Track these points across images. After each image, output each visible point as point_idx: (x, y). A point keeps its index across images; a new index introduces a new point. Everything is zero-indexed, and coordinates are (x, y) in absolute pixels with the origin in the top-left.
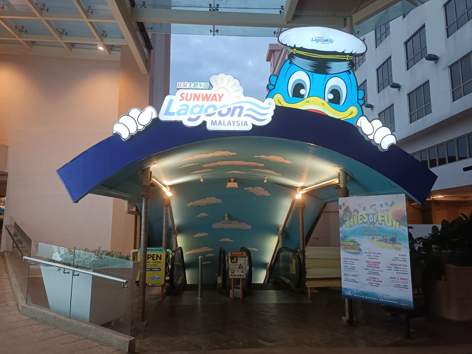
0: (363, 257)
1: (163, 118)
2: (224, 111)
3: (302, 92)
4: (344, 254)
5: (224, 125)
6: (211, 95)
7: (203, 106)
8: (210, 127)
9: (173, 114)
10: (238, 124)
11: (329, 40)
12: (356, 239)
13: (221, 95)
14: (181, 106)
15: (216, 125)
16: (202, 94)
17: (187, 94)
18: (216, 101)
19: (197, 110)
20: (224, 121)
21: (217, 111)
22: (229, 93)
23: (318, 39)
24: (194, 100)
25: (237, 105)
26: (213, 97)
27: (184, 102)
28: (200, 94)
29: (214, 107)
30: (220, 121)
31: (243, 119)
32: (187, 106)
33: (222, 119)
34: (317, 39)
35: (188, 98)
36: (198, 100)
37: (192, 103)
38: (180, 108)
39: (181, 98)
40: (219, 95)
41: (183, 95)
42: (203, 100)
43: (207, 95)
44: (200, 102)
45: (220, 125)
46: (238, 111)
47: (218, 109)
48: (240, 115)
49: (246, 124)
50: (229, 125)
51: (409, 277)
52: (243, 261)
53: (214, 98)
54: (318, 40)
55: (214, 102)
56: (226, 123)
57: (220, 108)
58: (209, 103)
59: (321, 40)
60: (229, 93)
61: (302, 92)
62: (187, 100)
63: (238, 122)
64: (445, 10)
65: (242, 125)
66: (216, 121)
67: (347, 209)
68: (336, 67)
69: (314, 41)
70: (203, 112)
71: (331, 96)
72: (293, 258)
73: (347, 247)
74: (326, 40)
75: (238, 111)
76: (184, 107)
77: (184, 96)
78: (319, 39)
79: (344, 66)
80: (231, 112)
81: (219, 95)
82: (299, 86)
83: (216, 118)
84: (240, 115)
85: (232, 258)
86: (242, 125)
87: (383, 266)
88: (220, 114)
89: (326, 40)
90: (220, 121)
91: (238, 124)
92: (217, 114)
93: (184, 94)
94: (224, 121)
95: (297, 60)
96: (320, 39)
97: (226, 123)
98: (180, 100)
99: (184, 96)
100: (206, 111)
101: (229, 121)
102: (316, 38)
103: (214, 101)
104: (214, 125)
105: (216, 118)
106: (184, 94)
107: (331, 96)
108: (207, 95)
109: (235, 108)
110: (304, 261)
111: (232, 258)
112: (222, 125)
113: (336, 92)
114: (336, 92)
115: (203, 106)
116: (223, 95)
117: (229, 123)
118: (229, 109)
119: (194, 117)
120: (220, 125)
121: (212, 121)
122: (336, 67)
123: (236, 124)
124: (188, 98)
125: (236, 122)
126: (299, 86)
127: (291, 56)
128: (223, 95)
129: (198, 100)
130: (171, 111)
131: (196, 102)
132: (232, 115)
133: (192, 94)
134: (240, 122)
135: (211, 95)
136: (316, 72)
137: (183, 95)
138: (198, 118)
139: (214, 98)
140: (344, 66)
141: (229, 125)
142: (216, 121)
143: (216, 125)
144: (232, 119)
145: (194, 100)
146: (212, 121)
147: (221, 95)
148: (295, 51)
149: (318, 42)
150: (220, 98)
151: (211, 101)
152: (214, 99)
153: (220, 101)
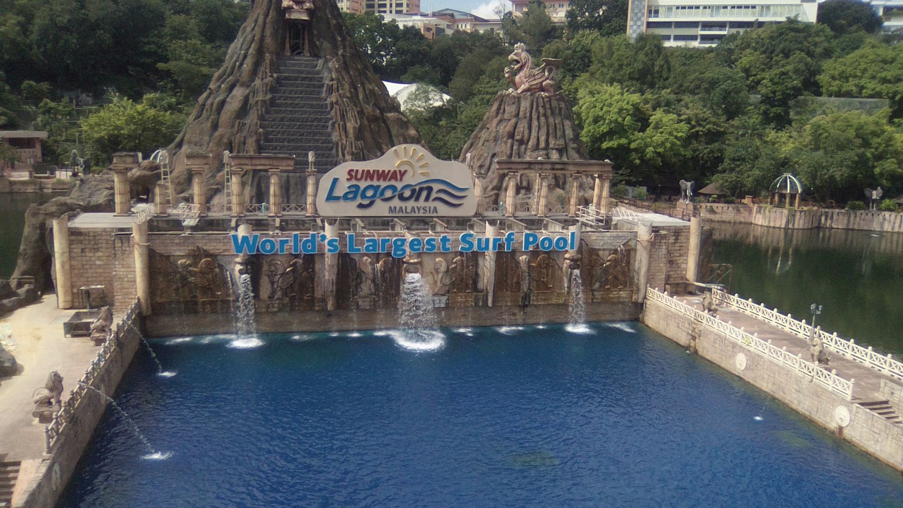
11: (436, 187)
14: (349, 187)
21: (397, 193)
23: (369, 183)
25: (425, 185)
27: (354, 182)
29: (394, 188)
30: (401, 208)
32: (357, 187)
34: (363, 184)
35: (359, 176)
36: (372, 179)
39: (349, 177)
42: (378, 179)
46: (424, 194)
48: (427, 199)
54: (370, 193)
55: (393, 183)
56: (409, 210)
58: (387, 183)
59: (388, 194)
64: (660, 27)
69: (345, 197)
70: (378, 195)
72: (610, 60)
74: (421, 190)
75: (424, 194)
76: (353, 189)
78: (375, 183)
84: (427, 199)
89: (421, 190)
90: (401, 208)
96: (383, 184)
97: (409, 210)
99: (353, 174)
100: (382, 194)
102: (354, 182)
115: (379, 186)
116: (405, 171)
117: (413, 209)
118: (413, 191)
121: (390, 207)
123: (422, 211)
128: (405, 171)
129: (372, 179)
131: (369, 183)
132: (417, 199)
134: (428, 209)
142: (395, 207)
146: (390, 207)
149: (366, 202)
151: (390, 180)
153: (401, 180)
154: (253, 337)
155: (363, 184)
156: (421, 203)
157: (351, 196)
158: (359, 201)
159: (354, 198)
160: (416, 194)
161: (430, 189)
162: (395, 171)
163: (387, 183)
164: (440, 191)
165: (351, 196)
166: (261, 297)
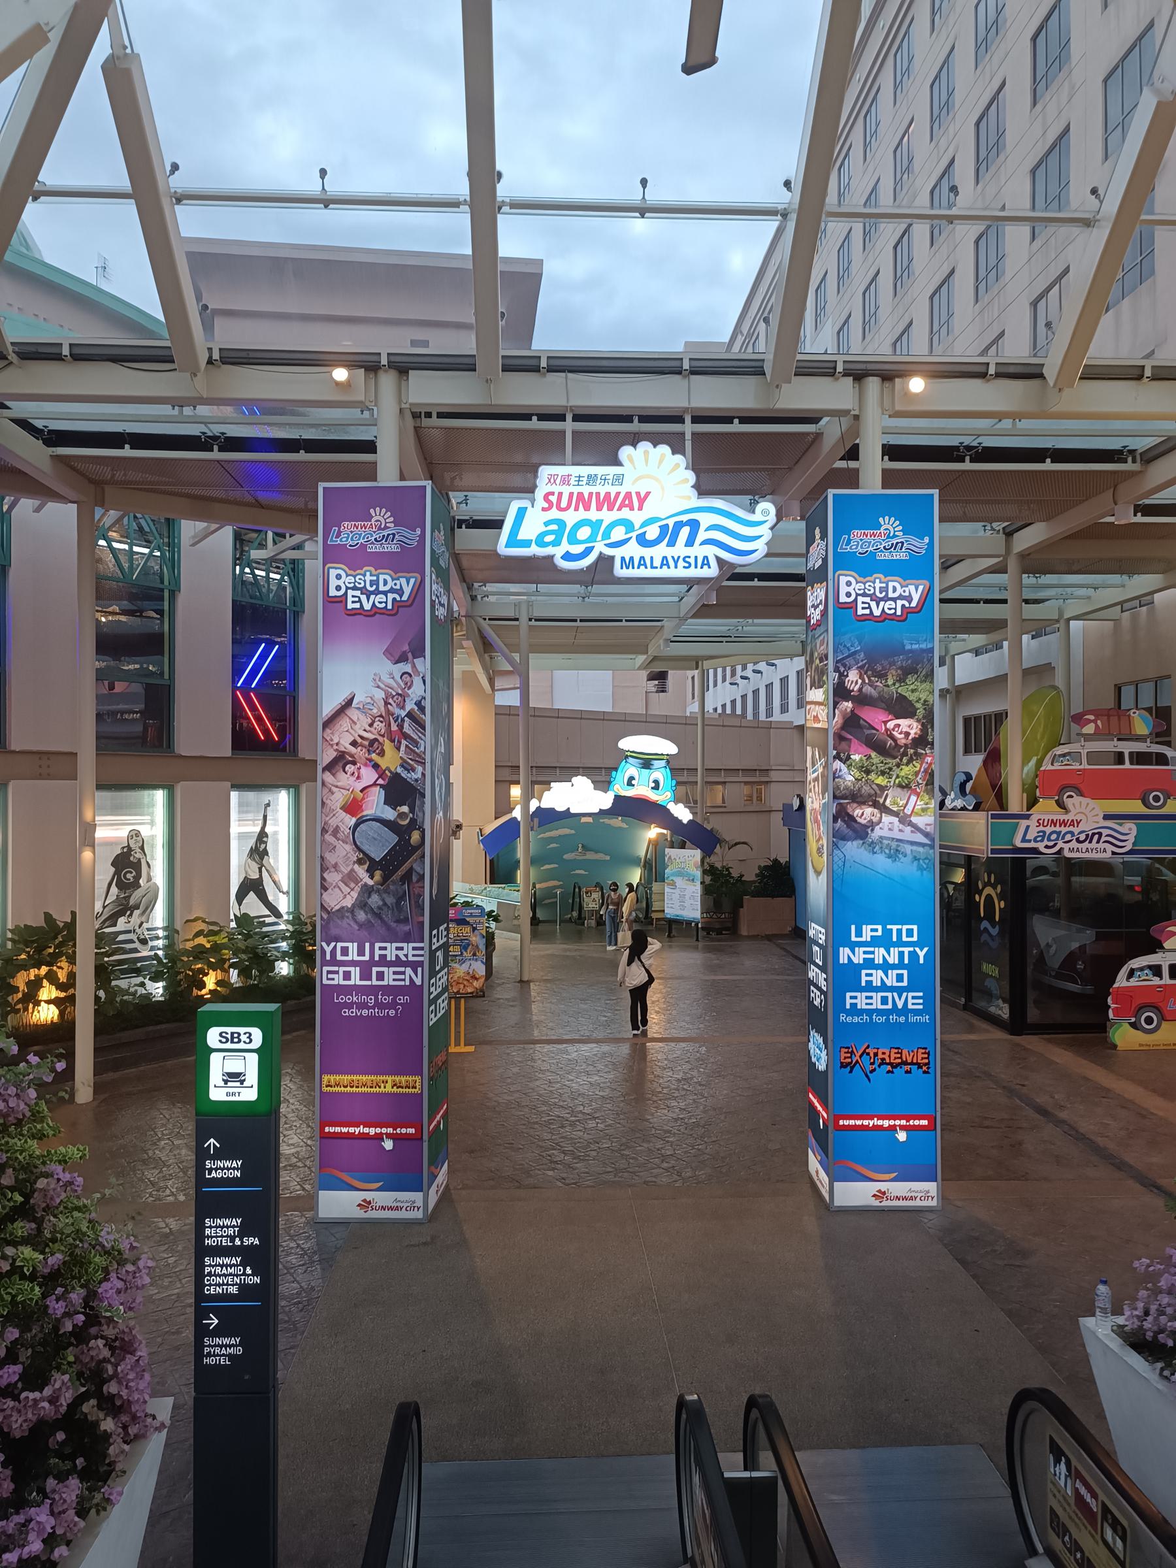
0: (677, 891)
1: (543, 806)
2: (652, 533)
3: (633, 782)
4: (667, 890)
5: (652, 567)
6: (618, 494)
7: (601, 521)
8: (572, 811)
9: (527, 543)
10: (687, 565)
11: (1105, 832)
12: (674, 878)
13: (642, 495)
14: (546, 524)
15: (633, 568)
16: (598, 494)
17: (560, 494)
18: (632, 509)
19: (584, 533)
20: (652, 558)
21: (634, 534)
22: (663, 489)
23: (1053, 828)
24: (576, 509)
25: (685, 518)
26: (624, 500)
27: (554, 514)
28: (591, 494)
30: (642, 558)
31: (699, 551)
32: (561, 523)
33: (647, 552)
34: (1048, 830)
35: (564, 504)
37: (571, 517)
38: (544, 529)
39: (546, 505)
40: (638, 494)
41: (551, 497)
43: (608, 494)
44: (593, 514)
45: (642, 567)
46: (685, 532)
47: (636, 528)
48: (690, 543)
49: (706, 562)
50: (665, 567)
51: (699, 903)
52: (596, 895)
53: (627, 502)
55: (626, 513)
56: (657, 563)
57: (642, 526)
58: (615, 515)
59: (1068, 837)
60: (663, 489)
61: (633, 782)
62: (559, 509)
63: (687, 559)
65: (696, 567)
66: (632, 558)
67: (670, 858)
68: (657, 764)
70: (599, 537)
71: (653, 785)
73: (669, 884)
75: (685, 532)
76: (554, 527)
77: (554, 499)
78: (1057, 829)
79: (663, 763)
80: (669, 534)
81: (638, 494)
82: (631, 778)
83: (633, 550)
84: (690, 543)
85: (587, 893)
86: (696, 567)
87: (687, 897)
88: (642, 541)
90: (642, 558)
91: (687, 565)
92: (634, 540)
93: (553, 494)
94: (652, 558)
95: (630, 760)
97: (657, 563)
98: (544, 509)
99: (554, 499)
100: (607, 535)
101: (665, 558)
102: (1041, 828)
103: (626, 510)
104: (628, 568)
105: (633, 550)
106: (553, 494)
107: (653, 785)
108: (608, 494)
109: (679, 526)
110: (651, 894)
111: (587, 893)
112: (646, 568)
113: (656, 782)
114: (656, 782)
115: (601, 521)
116: (648, 494)
117: (665, 562)
118: (664, 529)
119: (577, 549)
120: (642, 567)
121: (623, 559)
122: (657, 764)
123: (681, 563)
124: (564, 504)
125: (681, 559)
126: (631, 778)
127: (627, 757)
128: (648, 494)
130: (522, 536)
131: (582, 514)
132: (671, 543)
133: (571, 495)
134: (692, 560)
135: (618, 494)
136: (643, 768)
137: (551, 497)
138: (588, 551)
139: (627, 502)
140: (663, 763)
141: (665, 567)
142: (632, 558)
143: (633, 568)
144: (670, 552)
145: (576, 509)
146: (623, 559)
147: (642, 495)
148: (629, 754)
149: (1051, 844)
150: (642, 501)
151: (619, 509)
152: (626, 506)
153: (640, 508)
154: (696, 948)
155: (1048, 830)
156: (1094, 844)
157: (1039, 839)
158: (1046, 842)
159: (1042, 841)
160: (1089, 838)
161: (1100, 834)
162: (1073, 821)
163: (1067, 829)
164: (1107, 836)
165: (1039, 839)
166: (301, 755)
